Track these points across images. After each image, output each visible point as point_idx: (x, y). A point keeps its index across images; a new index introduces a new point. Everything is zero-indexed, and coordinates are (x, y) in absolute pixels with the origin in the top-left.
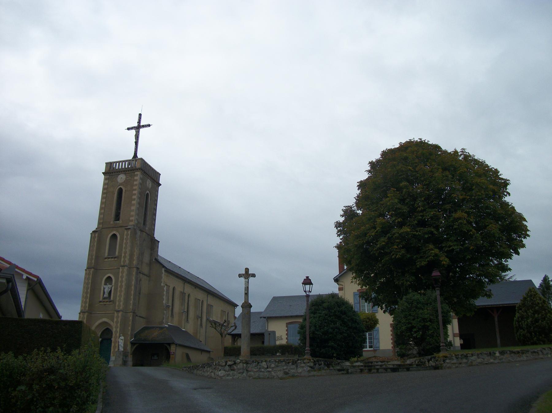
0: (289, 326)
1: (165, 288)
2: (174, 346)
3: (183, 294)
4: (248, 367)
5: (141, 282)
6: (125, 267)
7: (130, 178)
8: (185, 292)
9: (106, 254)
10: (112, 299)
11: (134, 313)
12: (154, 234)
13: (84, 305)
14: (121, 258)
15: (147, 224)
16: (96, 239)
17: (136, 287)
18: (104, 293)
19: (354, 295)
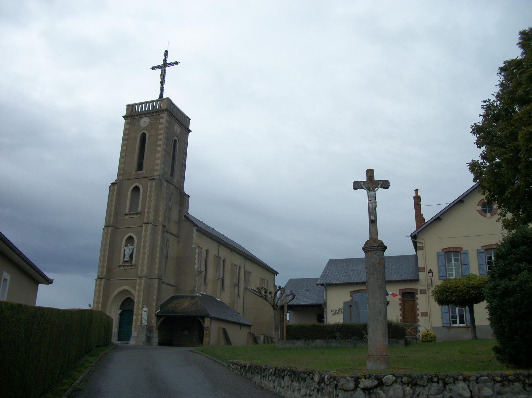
0: (354, 295)
1: (197, 251)
2: (209, 320)
3: (218, 257)
4: (418, 395)
5: (168, 243)
6: (149, 224)
7: (154, 121)
8: (220, 255)
9: (127, 211)
10: (134, 262)
11: (160, 279)
12: (183, 188)
13: (101, 270)
14: (144, 214)
15: (175, 175)
16: (115, 193)
17: (162, 249)
18: (124, 255)
19: (438, 256)
